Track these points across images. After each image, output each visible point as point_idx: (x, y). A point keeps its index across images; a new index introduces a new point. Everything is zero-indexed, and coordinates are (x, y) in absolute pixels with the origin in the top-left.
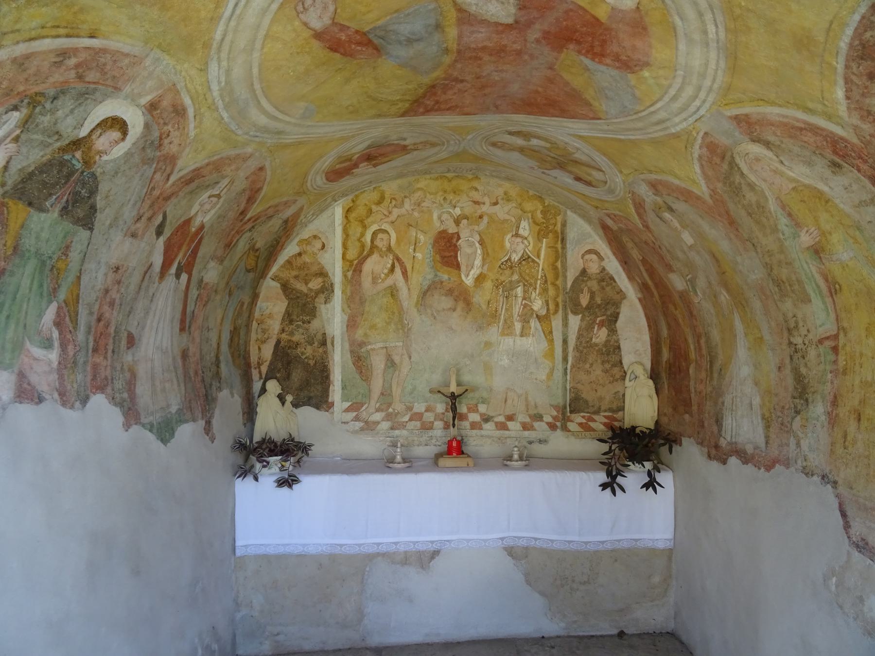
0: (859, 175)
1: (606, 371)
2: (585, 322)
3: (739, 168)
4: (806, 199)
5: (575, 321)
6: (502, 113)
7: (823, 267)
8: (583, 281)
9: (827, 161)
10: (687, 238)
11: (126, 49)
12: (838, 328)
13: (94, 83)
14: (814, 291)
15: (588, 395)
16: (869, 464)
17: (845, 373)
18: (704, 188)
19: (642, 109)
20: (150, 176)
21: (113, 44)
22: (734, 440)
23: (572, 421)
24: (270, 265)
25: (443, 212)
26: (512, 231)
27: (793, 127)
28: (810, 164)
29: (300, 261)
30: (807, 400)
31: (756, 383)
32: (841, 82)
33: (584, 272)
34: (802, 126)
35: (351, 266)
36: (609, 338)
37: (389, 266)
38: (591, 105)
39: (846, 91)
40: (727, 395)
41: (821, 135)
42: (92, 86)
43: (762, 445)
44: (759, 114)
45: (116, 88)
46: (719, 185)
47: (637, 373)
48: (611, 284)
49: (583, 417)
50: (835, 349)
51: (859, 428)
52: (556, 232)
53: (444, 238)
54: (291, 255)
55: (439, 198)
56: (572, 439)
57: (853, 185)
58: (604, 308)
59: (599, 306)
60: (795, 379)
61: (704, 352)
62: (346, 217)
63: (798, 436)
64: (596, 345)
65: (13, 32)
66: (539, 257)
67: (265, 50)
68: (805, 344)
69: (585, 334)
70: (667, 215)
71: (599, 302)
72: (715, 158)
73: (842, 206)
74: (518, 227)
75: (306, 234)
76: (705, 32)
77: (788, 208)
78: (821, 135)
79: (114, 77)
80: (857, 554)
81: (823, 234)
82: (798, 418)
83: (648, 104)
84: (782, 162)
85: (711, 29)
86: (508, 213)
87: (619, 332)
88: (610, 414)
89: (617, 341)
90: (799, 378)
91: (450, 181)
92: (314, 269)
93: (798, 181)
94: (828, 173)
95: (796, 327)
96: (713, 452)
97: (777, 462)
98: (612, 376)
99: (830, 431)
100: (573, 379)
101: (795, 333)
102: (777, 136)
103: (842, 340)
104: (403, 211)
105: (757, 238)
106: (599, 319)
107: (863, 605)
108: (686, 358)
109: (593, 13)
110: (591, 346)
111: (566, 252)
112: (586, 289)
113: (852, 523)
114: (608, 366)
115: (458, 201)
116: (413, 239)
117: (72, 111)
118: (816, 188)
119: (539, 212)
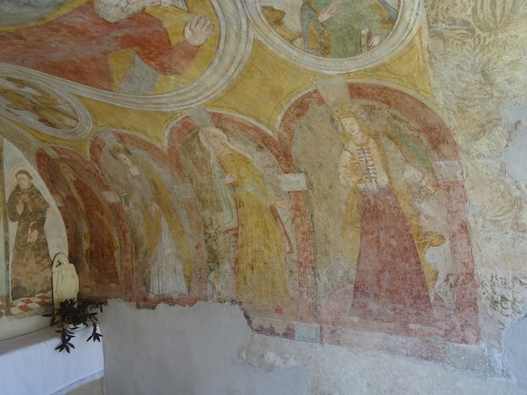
0: (271, 154)
1: (38, 263)
2: (21, 227)
3: (198, 138)
4: (236, 160)
5: (14, 227)
7: (235, 194)
8: (18, 195)
10: (134, 171)
12: (238, 224)
14: (226, 206)
15: (25, 283)
16: (261, 289)
17: (242, 246)
18: (166, 144)
19: (152, 94)
22: (161, 293)
23: (14, 306)
27: (246, 126)
28: (245, 144)
30: (218, 263)
31: (179, 257)
33: (18, 188)
36: (40, 237)
38: (112, 81)
40: (152, 267)
41: (259, 133)
43: (186, 292)
44: (228, 115)
47: (61, 261)
48: (38, 197)
49: (23, 301)
50: (236, 235)
51: (253, 273)
56: (15, 321)
58: (34, 215)
59: (31, 214)
60: (209, 252)
61: (129, 241)
63: (213, 283)
64: (31, 243)
68: (216, 233)
69: (22, 236)
70: (122, 156)
71: (31, 211)
73: (256, 166)
78: (259, 133)
80: (257, 334)
81: (240, 178)
82: (213, 273)
83: (158, 92)
84: (229, 140)
85: (232, 70)
87: (46, 232)
88: (42, 294)
89: (45, 239)
90: (211, 251)
93: (235, 151)
94: (254, 150)
95: (211, 224)
96: (142, 303)
97: (198, 300)
98: (42, 266)
99: (235, 277)
100: (14, 272)
101: (210, 228)
102: (234, 128)
103: (240, 230)
105: (196, 176)
106: (31, 223)
107: (264, 358)
108: (110, 246)
109: (170, 38)
110: (26, 244)
111: (3, 171)
112: (20, 201)
113: (253, 321)
114: (39, 258)
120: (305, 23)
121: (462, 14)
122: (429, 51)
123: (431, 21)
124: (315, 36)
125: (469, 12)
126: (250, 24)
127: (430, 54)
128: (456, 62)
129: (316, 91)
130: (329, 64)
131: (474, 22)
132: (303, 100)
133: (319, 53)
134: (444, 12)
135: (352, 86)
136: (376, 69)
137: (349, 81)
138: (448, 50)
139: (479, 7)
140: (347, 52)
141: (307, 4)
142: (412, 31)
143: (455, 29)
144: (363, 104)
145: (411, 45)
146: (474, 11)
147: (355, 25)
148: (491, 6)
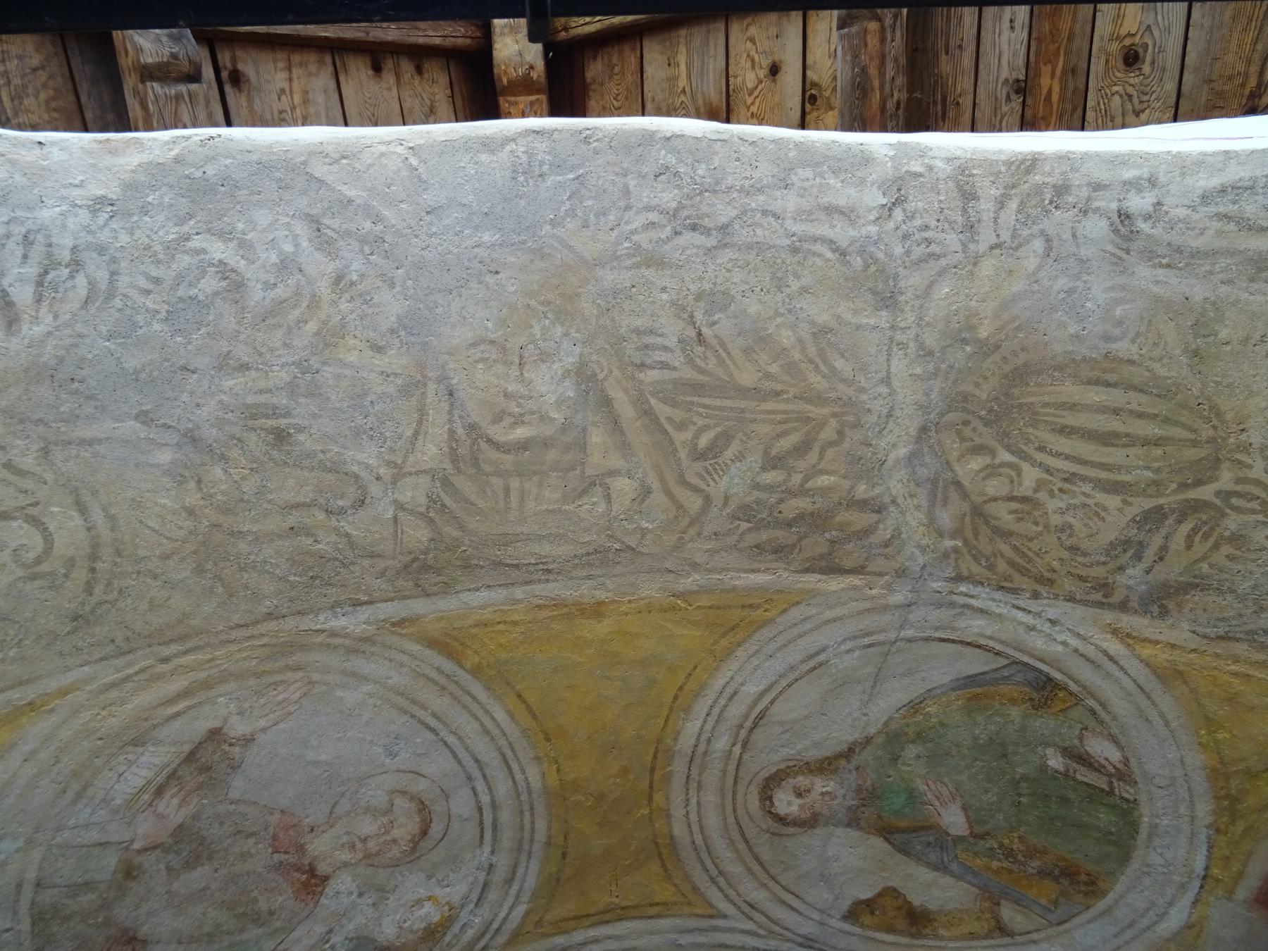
121: (1109, 519)
122: (1221, 638)
124: (1010, 871)
125: (1112, 501)
131: (1159, 494)
133: (1080, 898)
134: (1080, 559)
137: (1242, 893)
138: (1244, 586)
139: (1103, 475)
141: (891, 833)
142: (1112, 652)
143: (1164, 549)
145: (1169, 676)
147: (1020, 770)
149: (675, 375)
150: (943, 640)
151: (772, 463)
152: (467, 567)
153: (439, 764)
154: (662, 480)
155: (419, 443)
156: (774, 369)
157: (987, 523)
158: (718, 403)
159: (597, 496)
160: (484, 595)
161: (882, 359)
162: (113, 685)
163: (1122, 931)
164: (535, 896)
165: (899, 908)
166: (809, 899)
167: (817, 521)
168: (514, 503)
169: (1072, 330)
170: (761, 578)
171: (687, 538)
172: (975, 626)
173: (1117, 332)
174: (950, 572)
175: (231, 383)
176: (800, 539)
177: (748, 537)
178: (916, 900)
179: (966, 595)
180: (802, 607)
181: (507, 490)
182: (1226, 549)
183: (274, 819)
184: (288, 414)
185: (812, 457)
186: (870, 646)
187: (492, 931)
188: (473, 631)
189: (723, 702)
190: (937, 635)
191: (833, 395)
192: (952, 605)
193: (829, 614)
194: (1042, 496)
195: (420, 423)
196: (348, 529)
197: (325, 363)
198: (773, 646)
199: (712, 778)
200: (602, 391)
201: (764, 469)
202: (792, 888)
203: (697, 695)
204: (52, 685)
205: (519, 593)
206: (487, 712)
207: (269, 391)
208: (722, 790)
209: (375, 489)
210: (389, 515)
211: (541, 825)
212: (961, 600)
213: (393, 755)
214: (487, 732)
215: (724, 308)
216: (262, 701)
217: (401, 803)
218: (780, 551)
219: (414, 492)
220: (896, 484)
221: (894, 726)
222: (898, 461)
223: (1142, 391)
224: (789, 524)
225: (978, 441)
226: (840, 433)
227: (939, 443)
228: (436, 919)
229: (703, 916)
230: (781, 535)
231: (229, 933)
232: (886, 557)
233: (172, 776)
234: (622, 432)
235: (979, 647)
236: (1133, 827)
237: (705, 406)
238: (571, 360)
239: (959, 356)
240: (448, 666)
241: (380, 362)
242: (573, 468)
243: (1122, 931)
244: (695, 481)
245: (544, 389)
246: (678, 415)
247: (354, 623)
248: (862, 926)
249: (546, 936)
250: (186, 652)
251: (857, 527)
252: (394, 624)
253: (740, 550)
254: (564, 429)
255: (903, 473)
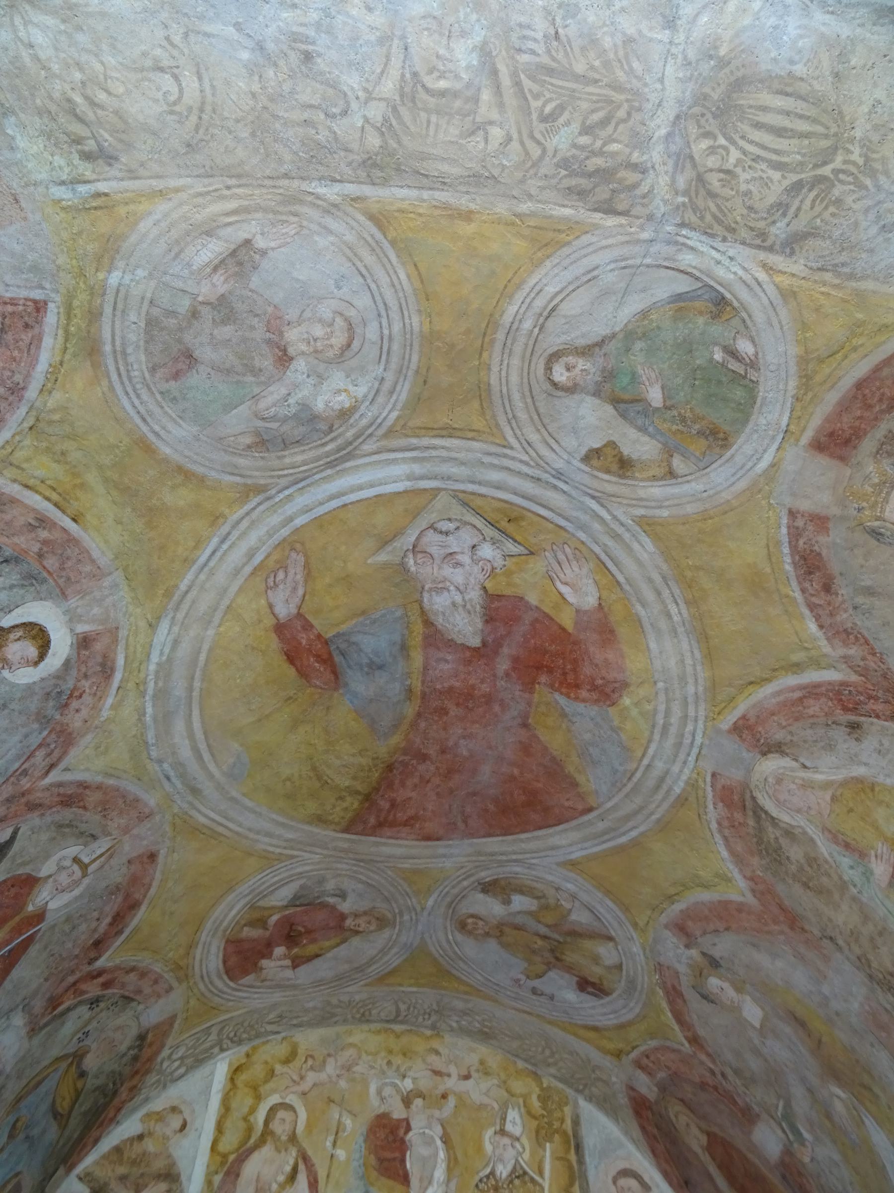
3: (766, 812)
4: (851, 805)
6: (472, 835)
9: (843, 728)
11: (95, 554)
13: (48, 572)
20: (33, 748)
21: (91, 541)
24: (85, 1146)
25: (386, 1084)
26: (494, 1124)
29: (137, 1148)
32: (806, 612)
34: (798, 694)
35: (223, 1164)
37: (288, 1169)
39: (817, 620)
42: (45, 574)
45: (63, 593)
46: (755, 861)
52: (565, 1133)
53: (385, 1126)
54: (126, 1137)
55: (381, 1062)
57: (884, 741)
62: (232, 1080)
65: (18, 467)
66: (541, 1173)
67: (221, 629)
72: (735, 814)
74: (504, 1119)
75: (158, 1104)
76: (669, 616)
77: (841, 837)
79: (69, 579)
84: (805, 767)
86: (487, 1094)
91: (398, 1036)
92: (158, 1165)
102: (784, 727)
104: (323, 1076)
115: (410, 1068)
116: (335, 1123)
117: (12, 587)
118: (852, 778)
119: (534, 1097)
120: (651, 429)
121: (773, 188)
122: (819, 269)
123: (758, 242)
124: (682, 432)
125: (776, 175)
126: (605, 502)
127: (827, 271)
128: (874, 230)
129: (792, 514)
130: (748, 449)
131: (802, 172)
132: (799, 552)
133: (717, 450)
134: (753, 215)
135: (819, 442)
136: (806, 380)
137: (805, 439)
138: (837, 233)
139: (774, 157)
140: (740, 404)
141: (618, 402)
142: (760, 279)
143: (799, 209)
144: (874, 450)
145: (788, 295)
146: (778, 166)
147: (698, 362)
148: (785, 137)
149: (538, 59)
150: (667, 268)
151: (586, 130)
152: (398, 169)
153: (363, 301)
154: (520, 132)
155: (384, 79)
156: (597, 63)
157: (704, 186)
158: (560, 83)
159: (479, 137)
160: (404, 192)
161: (661, 64)
162: (200, 194)
163: (738, 471)
164: (404, 408)
165: (615, 456)
166: (563, 444)
167: (605, 175)
168: (432, 133)
169: (773, 55)
170: (567, 212)
171: (528, 175)
172: (687, 259)
173: (797, 58)
174: (678, 220)
175: (286, 15)
176: (594, 187)
177: (564, 181)
178: (626, 451)
179: (685, 237)
180: (589, 236)
181: (429, 122)
182: (832, 209)
183: (270, 310)
184: (313, 43)
185: (610, 129)
186: (625, 268)
187: (376, 424)
188: (396, 214)
189: (532, 295)
190: (666, 264)
191: (628, 86)
192: (676, 243)
193: (604, 243)
194: (739, 170)
195: (386, 65)
196: (336, 129)
197: (339, 13)
198: (568, 261)
199: (518, 348)
200: (494, 64)
201: (580, 134)
202: (555, 435)
203: (519, 287)
204: (173, 183)
205: (426, 195)
206: (396, 272)
207: (305, 25)
208: (523, 357)
209: (354, 105)
210: (360, 125)
211: (415, 358)
212: (681, 240)
213: (339, 288)
214: (394, 286)
215: (574, 16)
216: (274, 230)
217: (339, 321)
218: (582, 194)
219: (376, 112)
220: (656, 154)
221: (630, 327)
222: (659, 138)
223: (804, 100)
224: (590, 175)
225: (708, 128)
226: (629, 114)
227: (685, 128)
228: (347, 405)
229: (499, 445)
230: (584, 182)
231: (237, 374)
232: (643, 205)
233: (222, 262)
234: (501, 96)
235: (687, 274)
236: (753, 399)
237: (552, 85)
238: (478, 39)
239: (706, 67)
240: (379, 236)
241: (370, 19)
242: (468, 115)
243: (738, 471)
244: (538, 136)
245: (460, 56)
246: (536, 88)
247: (330, 192)
248: (592, 467)
249: (407, 436)
250: (239, 186)
251: (628, 183)
252: (352, 199)
253: (558, 190)
254: (469, 85)
255: (660, 148)
